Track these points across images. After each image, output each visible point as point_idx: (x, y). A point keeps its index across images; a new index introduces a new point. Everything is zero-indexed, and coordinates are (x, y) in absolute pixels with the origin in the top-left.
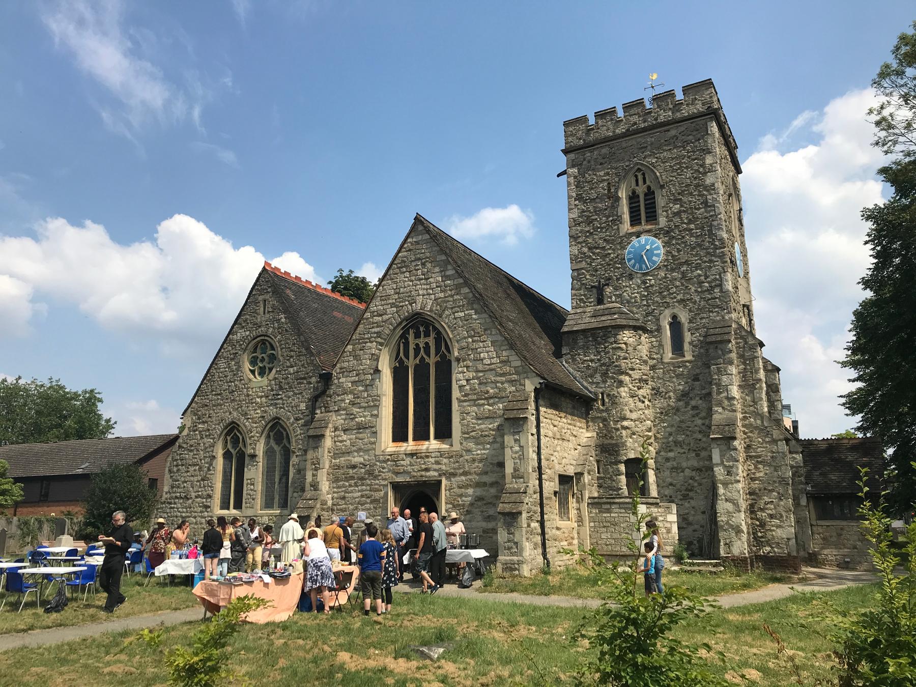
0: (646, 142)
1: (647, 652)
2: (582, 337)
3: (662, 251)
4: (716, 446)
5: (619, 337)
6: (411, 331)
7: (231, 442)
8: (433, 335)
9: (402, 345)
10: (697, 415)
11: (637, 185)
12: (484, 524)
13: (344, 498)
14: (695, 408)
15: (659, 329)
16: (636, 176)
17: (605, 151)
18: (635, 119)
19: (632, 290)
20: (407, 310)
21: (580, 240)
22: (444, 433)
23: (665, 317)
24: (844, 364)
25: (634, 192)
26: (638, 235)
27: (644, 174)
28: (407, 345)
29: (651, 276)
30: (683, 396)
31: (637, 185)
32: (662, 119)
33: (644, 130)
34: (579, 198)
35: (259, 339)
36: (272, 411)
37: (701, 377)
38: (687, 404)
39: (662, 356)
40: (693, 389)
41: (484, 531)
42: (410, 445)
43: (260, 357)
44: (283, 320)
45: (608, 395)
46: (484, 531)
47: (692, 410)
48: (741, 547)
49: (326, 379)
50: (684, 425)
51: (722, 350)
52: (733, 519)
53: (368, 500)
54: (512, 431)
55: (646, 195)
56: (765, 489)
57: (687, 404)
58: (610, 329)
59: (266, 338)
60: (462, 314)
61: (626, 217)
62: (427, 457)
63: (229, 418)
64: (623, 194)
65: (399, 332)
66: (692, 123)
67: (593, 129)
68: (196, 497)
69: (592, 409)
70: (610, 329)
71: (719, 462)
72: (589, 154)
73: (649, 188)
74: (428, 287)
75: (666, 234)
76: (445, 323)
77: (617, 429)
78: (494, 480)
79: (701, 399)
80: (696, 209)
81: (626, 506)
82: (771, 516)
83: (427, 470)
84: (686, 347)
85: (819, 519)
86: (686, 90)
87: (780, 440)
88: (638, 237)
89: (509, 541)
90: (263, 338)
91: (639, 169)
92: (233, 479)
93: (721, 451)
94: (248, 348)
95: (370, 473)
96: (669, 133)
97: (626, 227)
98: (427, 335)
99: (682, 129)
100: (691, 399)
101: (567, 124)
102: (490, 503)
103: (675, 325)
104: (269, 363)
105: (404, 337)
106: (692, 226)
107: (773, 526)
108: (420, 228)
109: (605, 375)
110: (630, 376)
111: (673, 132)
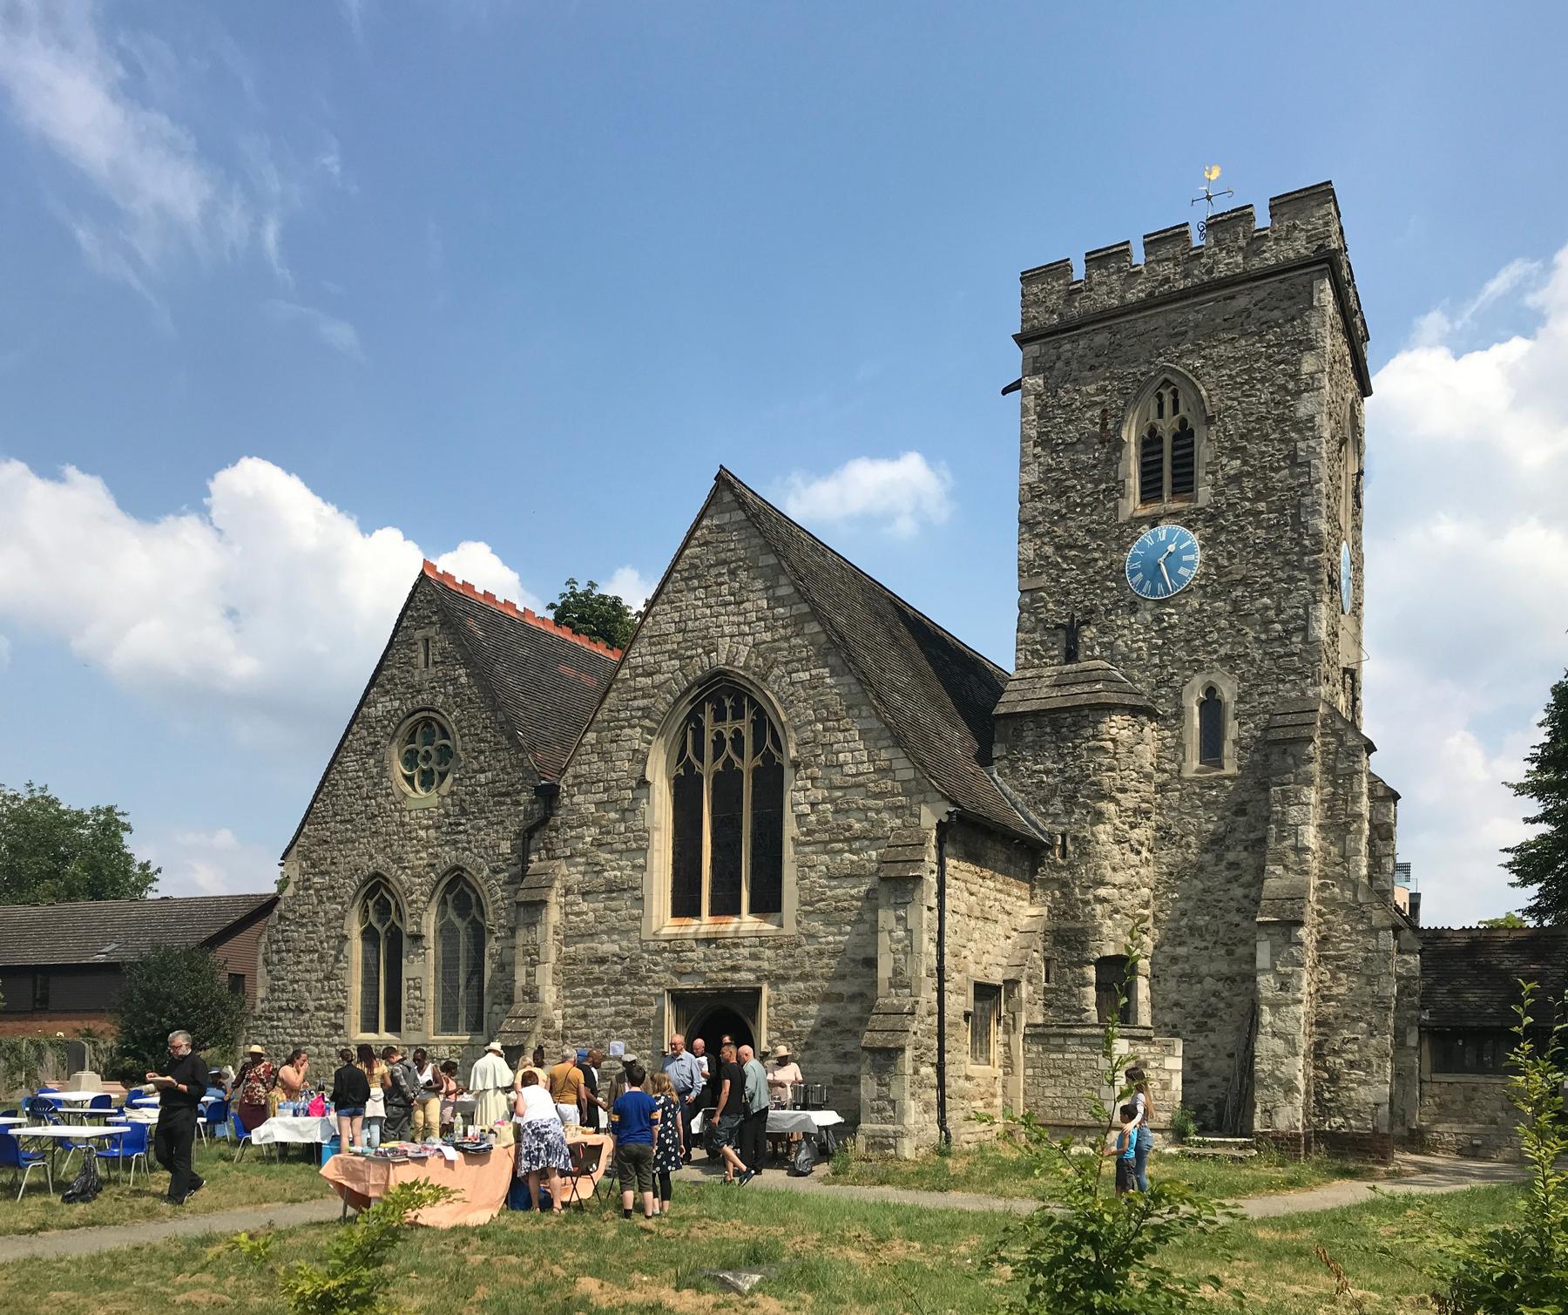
0: (1185, 323)
2: (1032, 725)
4: (1265, 937)
5: (1103, 727)
6: (708, 708)
7: (376, 911)
8: (749, 716)
9: (690, 733)
10: (1236, 878)
11: (1161, 415)
12: (837, 1068)
13: (584, 1016)
14: (1233, 865)
16: (1160, 396)
17: (1101, 339)
18: (1167, 269)
21: (1040, 529)
22: (767, 902)
23: (1192, 689)
25: (1152, 431)
26: (1154, 522)
27: (1175, 393)
29: (1172, 607)
30: (1213, 842)
31: (1161, 415)
32: (1221, 271)
33: (1184, 294)
34: (1043, 440)
35: (418, 716)
36: (449, 855)
37: (1249, 808)
38: (1219, 858)
39: (1180, 765)
40: (1233, 830)
41: (836, 1080)
42: (705, 924)
43: (422, 751)
44: (463, 680)
45: (1075, 838)
46: (836, 1080)
47: (1228, 869)
48: (1291, 1116)
50: (1209, 897)
51: (1294, 757)
52: (1283, 1068)
53: (629, 1022)
54: (892, 901)
55: (1176, 437)
56: (1346, 1016)
57: (1219, 858)
58: (1087, 712)
59: (432, 714)
60: (805, 676)
61: (1134, 483)
62: (736, 945)
63: (369, 867)
65: (685, 709)
66: (1281, 282)
67: (1079, 291)
68: (317, 1009)
69: (1042, 864)
70: (1087, 712)
71: (1268, 966)
72: (1068, 347)
73: (1183, 422)
74: (742, 619)
75: (1208, 521)
77: (1087, 903)
78: (856, 989)
79: (1246, 849)
80: (1273, 469)
81: (1092, 1041)
82: (1352, 1065)
83: (735, 969)
85: (365, 1030)
86: (1279, 205)
87: (1384, 929)
88: (1153, 525)
89: (880, 1098)
90: (425, 714)
91: (1166, 380)
92: (382, 978)
93: (1273, 946)
94: (399, 733)
95: (632, 973)
96: (1234, 303)
97: (1132, 504)
98: (738, 715)
99: (1261, 294)
100: (1228, 849)
101: (1028, 278)
102: (849, 1031)
104: (439, 764)
106: (1262, 506)
107: (1352, 1081)
108: (727, 497)
109: (1070, 800)
110: (1118, 803)
111: (1242, 302)
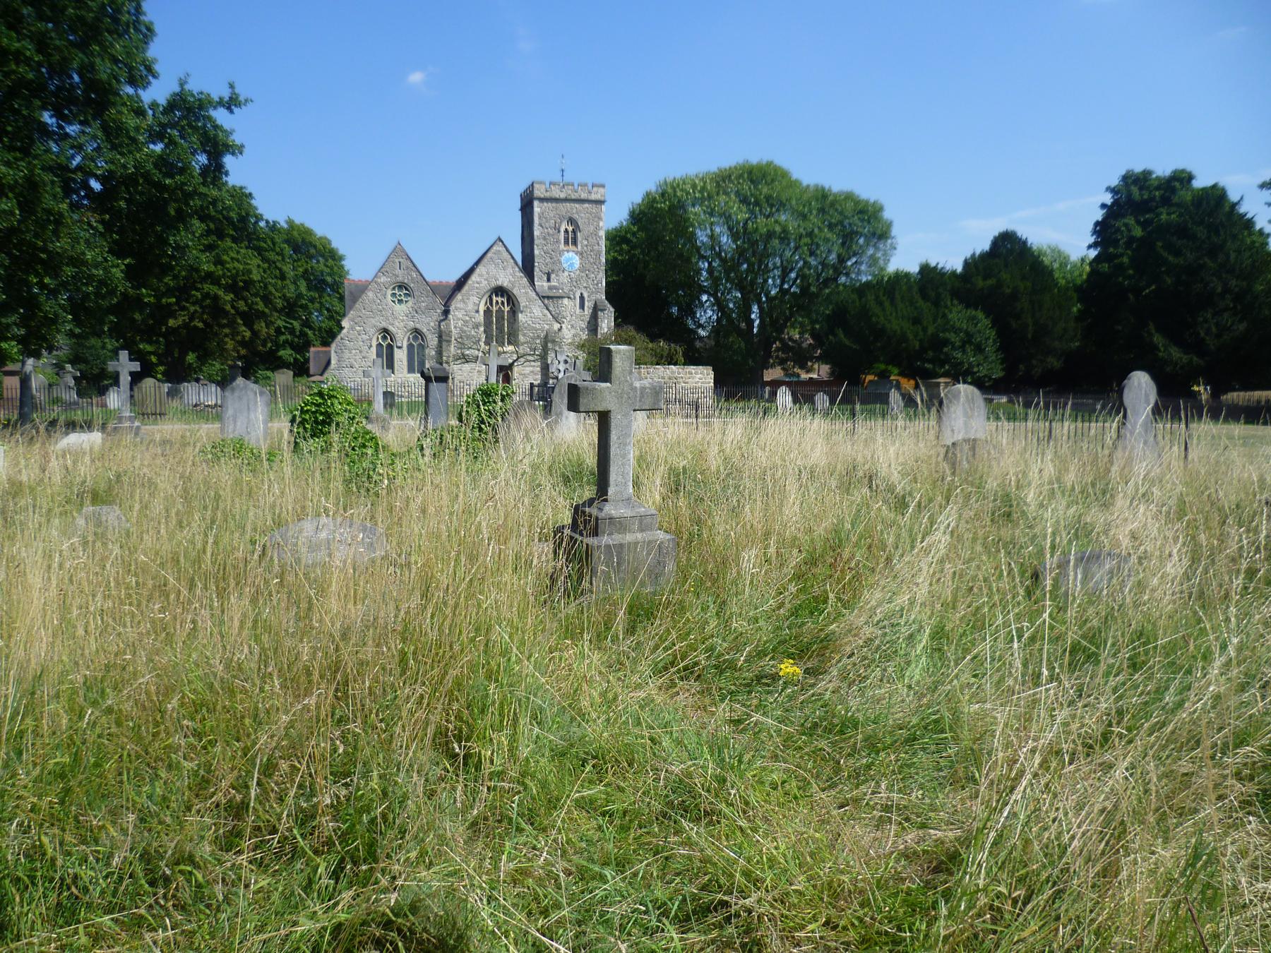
17: (554, 205)
19: (564, 277)
20: (494, 284)
63: (384, 325)
64: (562, 229)
65: (487, 296)
75: (581, 254)
97: (562, 246)
103: (582, 298)
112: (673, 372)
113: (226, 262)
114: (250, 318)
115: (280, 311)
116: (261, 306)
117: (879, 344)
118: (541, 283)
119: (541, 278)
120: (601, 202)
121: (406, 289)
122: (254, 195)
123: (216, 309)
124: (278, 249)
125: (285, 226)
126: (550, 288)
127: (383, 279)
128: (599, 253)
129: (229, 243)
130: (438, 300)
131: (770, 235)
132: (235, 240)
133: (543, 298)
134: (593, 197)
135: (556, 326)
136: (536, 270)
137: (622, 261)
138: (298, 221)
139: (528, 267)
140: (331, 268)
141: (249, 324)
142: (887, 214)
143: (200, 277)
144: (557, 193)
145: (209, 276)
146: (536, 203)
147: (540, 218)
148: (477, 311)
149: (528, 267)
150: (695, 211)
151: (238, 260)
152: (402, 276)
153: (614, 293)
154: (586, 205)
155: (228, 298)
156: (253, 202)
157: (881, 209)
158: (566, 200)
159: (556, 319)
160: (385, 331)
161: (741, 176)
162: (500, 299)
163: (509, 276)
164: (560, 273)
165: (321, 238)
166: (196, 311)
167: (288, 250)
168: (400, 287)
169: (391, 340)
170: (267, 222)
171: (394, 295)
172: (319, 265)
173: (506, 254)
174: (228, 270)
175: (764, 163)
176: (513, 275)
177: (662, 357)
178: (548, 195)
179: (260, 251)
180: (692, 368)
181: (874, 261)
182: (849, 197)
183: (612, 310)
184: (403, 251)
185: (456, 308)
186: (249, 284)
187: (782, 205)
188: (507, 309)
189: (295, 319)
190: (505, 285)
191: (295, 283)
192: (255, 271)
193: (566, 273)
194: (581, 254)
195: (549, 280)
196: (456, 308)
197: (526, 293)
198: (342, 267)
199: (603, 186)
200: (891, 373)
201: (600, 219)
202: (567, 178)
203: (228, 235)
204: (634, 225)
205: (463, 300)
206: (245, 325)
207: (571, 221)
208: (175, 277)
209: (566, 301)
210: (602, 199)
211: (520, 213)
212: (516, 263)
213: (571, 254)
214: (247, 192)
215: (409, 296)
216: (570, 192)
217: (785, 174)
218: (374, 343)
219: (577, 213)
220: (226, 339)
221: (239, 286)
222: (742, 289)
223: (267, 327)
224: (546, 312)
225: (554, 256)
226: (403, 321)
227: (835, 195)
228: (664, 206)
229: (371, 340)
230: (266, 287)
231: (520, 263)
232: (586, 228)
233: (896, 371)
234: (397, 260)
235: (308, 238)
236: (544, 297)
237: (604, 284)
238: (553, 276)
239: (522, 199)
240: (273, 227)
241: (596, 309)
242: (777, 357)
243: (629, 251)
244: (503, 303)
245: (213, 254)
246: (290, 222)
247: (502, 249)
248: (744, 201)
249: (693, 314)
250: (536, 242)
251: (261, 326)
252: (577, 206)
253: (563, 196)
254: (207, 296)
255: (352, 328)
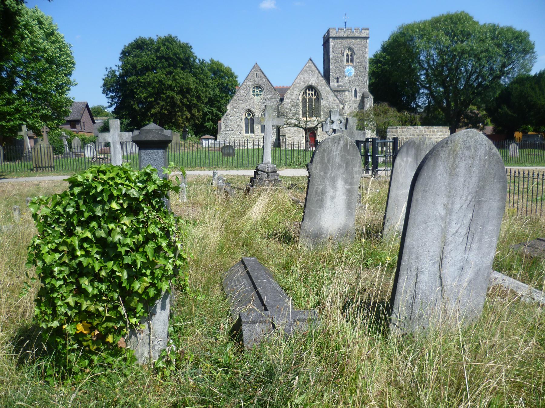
1: (107, 286)
3: (354, 72)
15: (352, 91)
17: (340, 40)
19: (346, 80)
20: (307, 84)
24: (103, 80)
28: (306, 93)
49: (282, 100)
63: (249, 107)
64: (345, 54)
65: (303, 90)
75: (355, 67)
76: (319, 88)
84: (358, 96)
97: (345, 63)
103: (356, 91)
105: (305, 91)
112: (421, 131)
113: (177, 79)
114: (189, 108)
115: (206, 104)
116: (195, 101)
117: (532, 113)
118: (333, 84)
119: (333, 81)
120: (367, 38)
121: (260, 88)
122: (193, 47)
123: (173, 104)
124: (205, 74)
125: (210, 62)
126: (338, 86)
127: (248, 83)
128: (365, 66)
129: (179, 70)
130: (277, 93)
131: (463, 52)
132: (183, 69)
133: (334, 91)
134: (362, 35)
135: (342, 106)
136: (331, 76)
137: (378, 72)
138: (215, 60)
139: (327, 76)
140: (231, 82)
141: (190, 110)
142: (532, 39)
143: (165, 88)
144: (342, 34)
145: (170, 87)
146: (331, 40)
147: (333, 48)
148: (298, 99)
149: (327, 76)
150: (420, 43)
151: (183, 79)
152: (258, 81)
153: (373, 88)
154: (358, 40)
155: (178, 98)
156: (192, 50)
157: (528, 35)
158: (347, 38)
159: (341, 102)
160: (249, 111)
161: (446, 20)
162: (310, 92)
163: (316, 80)
164: (344, 78)
165: (226, 67)
166: (163, 105)
167: (210, 74)
168: (257, 87)
169: (253, 115)
170: (199, 60)
171: (254, 91)
172: (225, 81)
173: (313, 67)
174: (178, 83)
175: (459, 13)
176: (318, 79)
177: (406, 122)
178: (337, 35)
179: (195, 75)
180: (435, 128)
181: (524, 67)
182: (509, 29)
183: (372, 97)
184: (259, 67)
185: (287, 98)
186: (189, 90)
187: (469, 34)
188: (314, 97)
189: (214, 107)
190: (313, 84)
191: (213, 90)
192: (192, 84)
193: (347, 78)
194: (356, 67)
195: (338, 82)
196: (287, 98)
197: (325, 88)
198: (237, 81)
199: (368, 29)
200: (529, 130)
201: (366, 47)
202: (347, 27)
203: (179, 67)
204: (384, 53)
205: (290, 93)
206: (188, 111)
207: (350, 49)
208: (154, 88)
209: (347, 93)
210: (367, 36)
211: (322, 47)
212: (319, 72)
213: (350, 67)
214: (189, 45)
215: (262, 91)
216: (349, 33)
217: (471, 18)
218: (244, 117)
219: (353, 44)
220: (179, 118)
221: (184, 91)
222: (444, 87)
223: (198, 112)
224: (336, 98)
225: (341, 68)
226: (258, 105)
227: (502, 29)
228: (403, 39)
229: (242, 115)
230: (197, 92)
231: (323, 74)
232: (358, 53)
233: (531, 129)
234: (255, 73)
235: (220, 68)
236: (335, 91)
237: (368, 83)
238: (340, 80)
239: (324, 40)
240: (202, 62)
241: (363, 97)
242: (464, 122)
243: (381, 67)
244: (312, 94)
245: (172, 76)
246: (212, 61)
247: (312, 65)
248: (447, 34)
249: (414, 99)
250: (331, 61)
251: (195, 111)
252: (353, 40)
253: (345, 35)
254: (168, 97)
255: (232, 110)
